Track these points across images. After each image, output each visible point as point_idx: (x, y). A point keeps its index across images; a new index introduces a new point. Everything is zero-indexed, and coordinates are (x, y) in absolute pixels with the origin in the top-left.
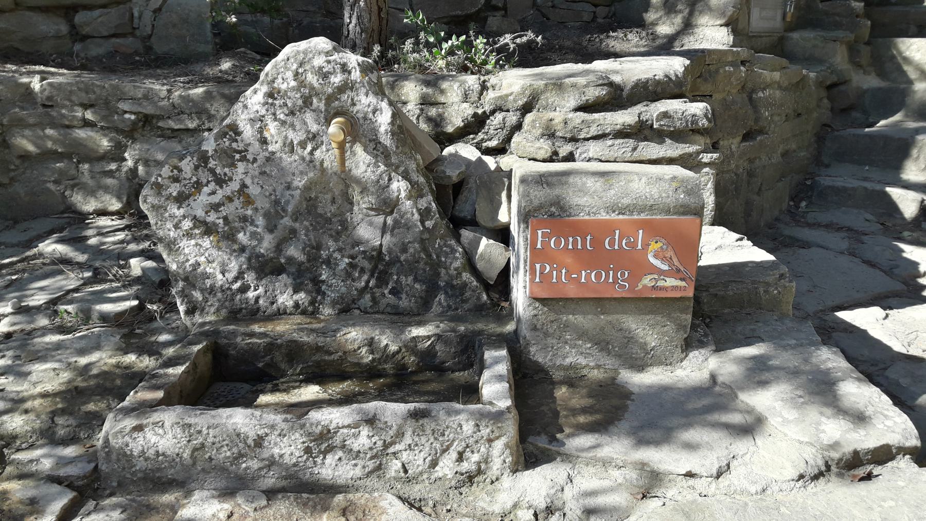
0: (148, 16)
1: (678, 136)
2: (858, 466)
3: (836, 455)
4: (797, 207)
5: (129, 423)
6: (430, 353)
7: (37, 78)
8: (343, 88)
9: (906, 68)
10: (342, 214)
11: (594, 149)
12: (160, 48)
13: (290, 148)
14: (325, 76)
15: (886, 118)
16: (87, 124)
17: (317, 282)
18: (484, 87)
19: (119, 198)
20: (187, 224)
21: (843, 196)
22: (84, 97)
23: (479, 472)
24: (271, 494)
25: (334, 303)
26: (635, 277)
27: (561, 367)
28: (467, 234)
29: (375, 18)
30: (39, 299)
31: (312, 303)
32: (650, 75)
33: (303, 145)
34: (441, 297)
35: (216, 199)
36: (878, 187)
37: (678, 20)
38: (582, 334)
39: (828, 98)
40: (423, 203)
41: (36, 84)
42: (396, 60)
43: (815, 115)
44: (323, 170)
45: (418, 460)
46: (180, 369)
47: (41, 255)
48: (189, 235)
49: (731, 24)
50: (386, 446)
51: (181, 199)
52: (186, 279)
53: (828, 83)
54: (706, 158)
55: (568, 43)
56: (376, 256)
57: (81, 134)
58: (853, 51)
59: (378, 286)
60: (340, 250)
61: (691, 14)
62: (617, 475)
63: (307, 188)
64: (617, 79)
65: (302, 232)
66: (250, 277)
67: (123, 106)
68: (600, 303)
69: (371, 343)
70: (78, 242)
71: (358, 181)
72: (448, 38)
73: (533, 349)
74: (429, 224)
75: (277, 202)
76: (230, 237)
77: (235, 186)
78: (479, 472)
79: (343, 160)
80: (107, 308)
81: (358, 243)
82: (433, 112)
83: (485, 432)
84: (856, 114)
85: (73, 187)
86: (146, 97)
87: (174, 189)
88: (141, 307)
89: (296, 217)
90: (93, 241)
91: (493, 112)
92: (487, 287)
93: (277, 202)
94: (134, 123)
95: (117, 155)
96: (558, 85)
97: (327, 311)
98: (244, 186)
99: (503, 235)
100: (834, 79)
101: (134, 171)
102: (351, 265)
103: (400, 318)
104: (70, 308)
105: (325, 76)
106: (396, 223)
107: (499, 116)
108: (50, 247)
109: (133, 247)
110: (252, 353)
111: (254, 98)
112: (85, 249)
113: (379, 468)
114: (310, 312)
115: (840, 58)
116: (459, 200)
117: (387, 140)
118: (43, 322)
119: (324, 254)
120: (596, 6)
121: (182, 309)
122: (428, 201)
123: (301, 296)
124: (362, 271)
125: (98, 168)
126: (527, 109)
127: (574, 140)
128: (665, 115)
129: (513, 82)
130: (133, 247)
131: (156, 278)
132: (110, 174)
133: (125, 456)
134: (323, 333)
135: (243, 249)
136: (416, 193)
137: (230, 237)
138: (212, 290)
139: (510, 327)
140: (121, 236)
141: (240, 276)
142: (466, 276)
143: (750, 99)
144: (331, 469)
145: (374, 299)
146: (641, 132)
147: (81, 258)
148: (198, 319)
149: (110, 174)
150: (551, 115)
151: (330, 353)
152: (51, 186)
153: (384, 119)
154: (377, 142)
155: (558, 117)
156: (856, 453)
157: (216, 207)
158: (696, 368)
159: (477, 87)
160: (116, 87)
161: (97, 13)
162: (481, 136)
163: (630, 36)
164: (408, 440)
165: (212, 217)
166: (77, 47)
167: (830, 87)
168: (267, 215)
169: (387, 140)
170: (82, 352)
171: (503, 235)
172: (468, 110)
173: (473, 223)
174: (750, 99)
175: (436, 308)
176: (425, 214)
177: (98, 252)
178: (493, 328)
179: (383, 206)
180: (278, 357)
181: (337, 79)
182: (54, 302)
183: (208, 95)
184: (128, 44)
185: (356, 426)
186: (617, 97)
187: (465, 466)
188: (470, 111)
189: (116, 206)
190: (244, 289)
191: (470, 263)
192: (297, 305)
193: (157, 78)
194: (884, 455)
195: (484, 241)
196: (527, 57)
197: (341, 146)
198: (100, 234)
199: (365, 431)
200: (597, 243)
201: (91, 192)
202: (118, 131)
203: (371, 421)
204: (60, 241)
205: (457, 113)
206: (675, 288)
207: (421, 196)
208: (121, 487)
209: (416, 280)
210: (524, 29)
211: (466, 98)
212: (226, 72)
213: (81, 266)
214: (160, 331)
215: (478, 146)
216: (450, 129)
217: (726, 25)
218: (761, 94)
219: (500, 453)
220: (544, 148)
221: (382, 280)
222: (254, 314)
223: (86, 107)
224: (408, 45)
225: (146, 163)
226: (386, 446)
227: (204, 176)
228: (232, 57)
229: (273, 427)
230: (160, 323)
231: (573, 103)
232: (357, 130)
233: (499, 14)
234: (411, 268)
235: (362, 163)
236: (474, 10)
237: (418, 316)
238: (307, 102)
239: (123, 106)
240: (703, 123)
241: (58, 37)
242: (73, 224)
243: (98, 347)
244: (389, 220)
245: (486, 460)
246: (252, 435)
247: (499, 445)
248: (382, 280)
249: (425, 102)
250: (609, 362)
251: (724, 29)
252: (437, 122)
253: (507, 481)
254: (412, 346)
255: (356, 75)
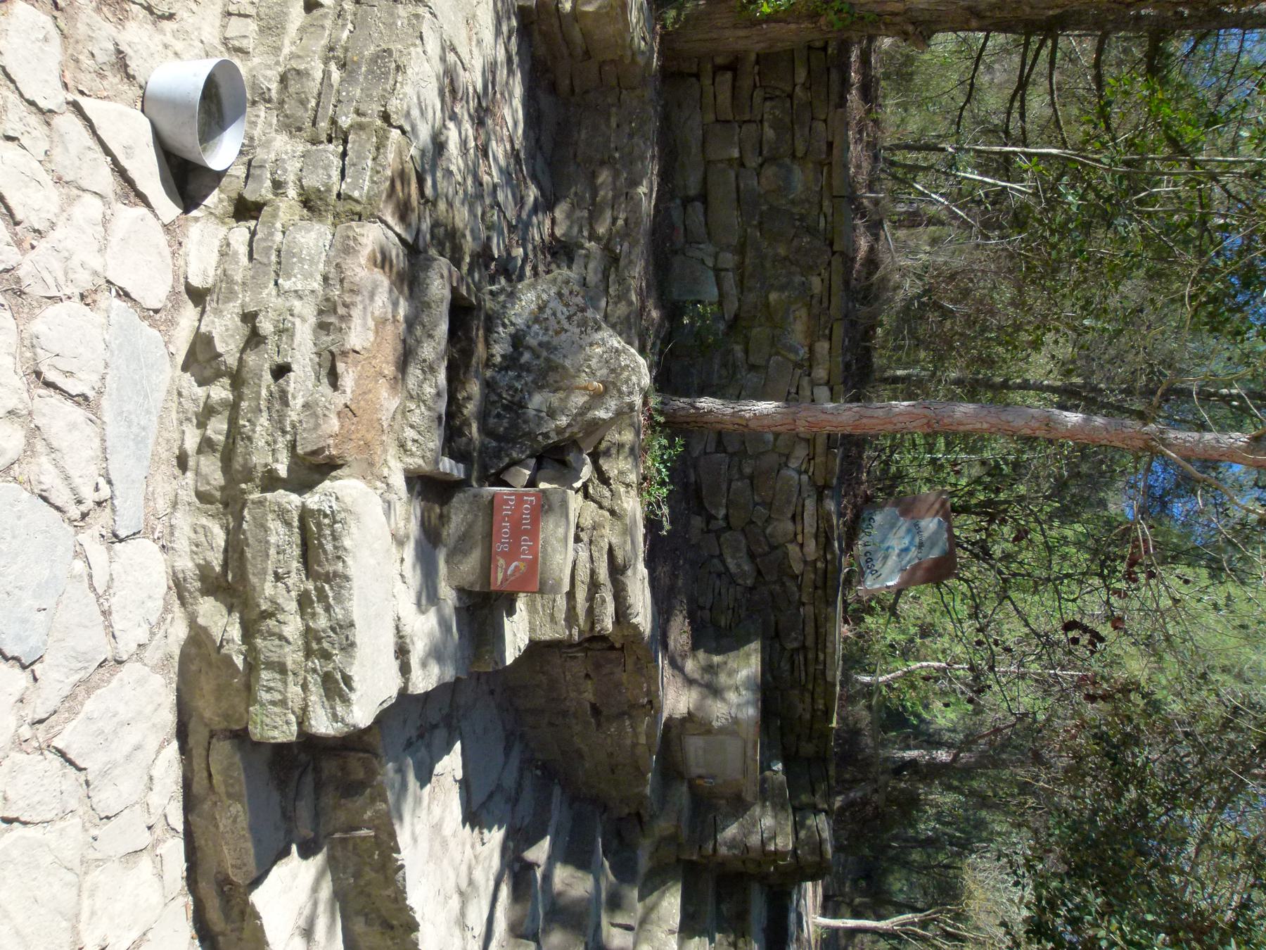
0: (698, 254)
1: (590, 611)
2: (402, 652)
3: (408, 641)
4: (537, 768)
5: (446, 273)
6: (462, 434)
7: (646, 190)
8: (619, 391)
9: (656, 894)
10: (548, 386)
11: (584, 555)
12: (677, 261)
13: (588, 358)
14: (626, 382)
15: (611, 867)
16: (614, 220)
17: (507, 369)
18: (628, 485)
19: (563, 235)
20: (545, 297)
21: (542, 806)
22: (632, 221)
23: (406, 451)
24: (404, 341)
25: (493, 378)
26: (503, 554)
27: (449, 512)
28: (533, 462)
29: (682, 419)
30: (500, 197)
31: (494, 365)
32: (630, 593)
33: (589, 367)
34: (494, 444)
35: (559, 314)
36: (551, 829)
37: (697, 676)
38: (470, 526)
39: (629, 814)
40: (553, 434)
41: (642, 189)
42: (654, 432)
43: (614, 794)
44: (574, 377)
45: (415, 418)
46: (465, 293)
47: (527, 187)
48: (539, 297)
49: (690, 717)
50: (424, 402)
51: (560, 295)
52: (512, 293)
53: (642, 811)
54: (575, 632)
55: (680, 583)
56: (522, 405)
57: (608, 214)
58: (672, 839)
59: (503, 405)
60: (526, 384)
61: (700, 685)
62: (402, 524)
63: (564, 367)
64: (629, 572)
65: (536, 363)
66: (512, 330)
67: (626, 245)
68: (489, 537)
69: (469, 398)
70: (535, 210)
71: (567, 397)
72: (666, 467)
73: (461, 495)
74: (540, 438)
75: (556, 349)
76: (536, 320)
77: (566, 326)
78: (406, 451)
79: (578, 388)
80: (495, 240)
81: (530, 394)
82: (614, 451)
83: (428, 454)
84: (615, 843)
85: (572, 204)
86: (631, 262)
87: (565, 291)
88: (493, 259)
89: (548, 360)
90: (535, 220)
91: (611, 490)
92: (498, 474)
93: (556, 349)
94: (613, 251)
95: (593, 237)
96: (628, 531)
97: (489, 373)
98: (566, 331)
99: (532, 483)
100: (646, 818)
101: (582, 247)
102: (517, 389)
103: (483, 416)
104: (495, 217)
105: (626, 382)
106: (542, 418)
107: (608, 494)
108: (532, 193)
109: (530, 247)
110: (468, 330)
111: (616, 342)
112: (529, 216)
113: (412, 397)
114: (488, 363)
115: (664, 826)
116: (555, 458)
117: (590, 415)
118: (488, 201)
119: (524, 374)
120: (711, 609)
121: (493, 288)
122: (554, 438)
123: (498, 359)
124: (513, 396)
125: (584, 222)
126: (612, 512)
127: (591, 542)
128: (604, 601)
129: (632, 505)
130: (530, 247)
131: (510, 267)
132: (581, 231)
133: (427, 268)
134: (477, 371)
135: (529, 327)
136: (560, 431)
137: (536, 320)
138: (504, 307)
139: (474, 484)
140: (537, 237)
141: (513, 324)
142: (507, 460)
143: (624, 713)
144: (414, 372)
145: (494, 402)
146: (594, 586)
147: (524, 216)
148: (487, 297)
149: (581, 231)
150: (607, 528)
151: (465, 373)
152: (573, 190)
153: (602, 414)
154: (589, 409)
155: (606, 531)
156: (408, 652)
157: (554, 314)
158: (447, 594)
159: (628, 481)
160: (637, 242)
161: (702, 219)
162: (596, 482)
163: (685, 636)
164: (426, 413)
165: (548, 312)
166: (678, 201)
167: (638, 815)
168: (549, 343)
169: (590, 415)
170: (472, 231)
171: (532, 483)
172: (613, 473)
173: (539, 467)
174: (624, 713)
175: (487, 440)
176: (546, 436)
177: (528, 225)
178: (475, 474)
179: (554, 411)
180: (464, 344)
181: (624, 388)
182: (499, 205)
183: (630, 303)
184: (680, 238)
185: (436, 386)
186: (617, 571)
187: (410, 443)
188: (611, 475)
189: (558, 232)
190: (504, 326)
191: (514, 463)
192: (493, 356)
193: (646, 268)
194: (405, 669)
195: (528, 472)
196: (652, 524)
197: (586, 388)
198: (539, 223)
199: (433, 391)
200: (526, 532)
201: (569, 216)
202: (609, 240)
203: (438, 394)
204: (536, 199)
205: (612, 467)
206: (496, 578)
207: (558, 434)
208: (411, 265)
209: (506, 429)
210: (671, 523)
211: (621, 473)
212: (649, 313)
213: (519, 216)
214: (480, 273)
215: (590, 480)
216: (601, 461)
217: (689, 713)
218: (627, 723)
219: (416, 462)
220: (587, 522)
221: (505, 408)
222: (489, 330)
223: (626, 220)
224: (665, 442)
225: (587, 256)
226: (424, 402)
227: (573, 309)
228: (662, 319)
229: (439, 344)
230: (485, 273)
231: (614, 541)
232: (597, 398)
233: (703, 526)
234: (514, 425)
235: (579, 400)
236: (706, 505)
237: (483, 429)
238: (613, 371)
239: (626, 245)
240: (598, 628)
241: (685, 187)
242: (547, 204)
243: (474, 239)
244: (543, 414)
245: (412, 455)
246: (435, 333)
247: (421, 462)
248: (505, 408)
249: (621, 446)
250: (451, 542)
251: (685, 711)
252: (607, 453)
253: (400, 466)
254: (466, 423)
255: (627, 400)
